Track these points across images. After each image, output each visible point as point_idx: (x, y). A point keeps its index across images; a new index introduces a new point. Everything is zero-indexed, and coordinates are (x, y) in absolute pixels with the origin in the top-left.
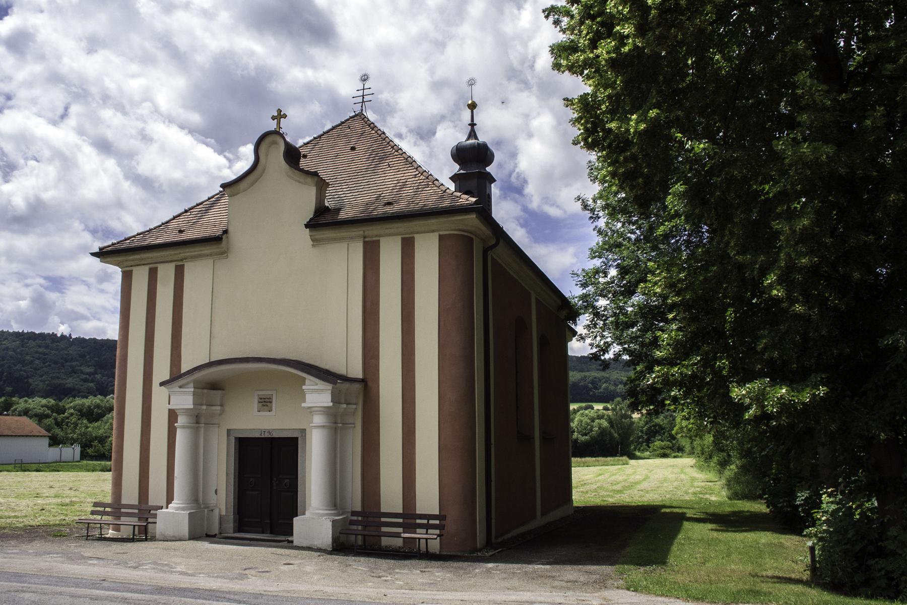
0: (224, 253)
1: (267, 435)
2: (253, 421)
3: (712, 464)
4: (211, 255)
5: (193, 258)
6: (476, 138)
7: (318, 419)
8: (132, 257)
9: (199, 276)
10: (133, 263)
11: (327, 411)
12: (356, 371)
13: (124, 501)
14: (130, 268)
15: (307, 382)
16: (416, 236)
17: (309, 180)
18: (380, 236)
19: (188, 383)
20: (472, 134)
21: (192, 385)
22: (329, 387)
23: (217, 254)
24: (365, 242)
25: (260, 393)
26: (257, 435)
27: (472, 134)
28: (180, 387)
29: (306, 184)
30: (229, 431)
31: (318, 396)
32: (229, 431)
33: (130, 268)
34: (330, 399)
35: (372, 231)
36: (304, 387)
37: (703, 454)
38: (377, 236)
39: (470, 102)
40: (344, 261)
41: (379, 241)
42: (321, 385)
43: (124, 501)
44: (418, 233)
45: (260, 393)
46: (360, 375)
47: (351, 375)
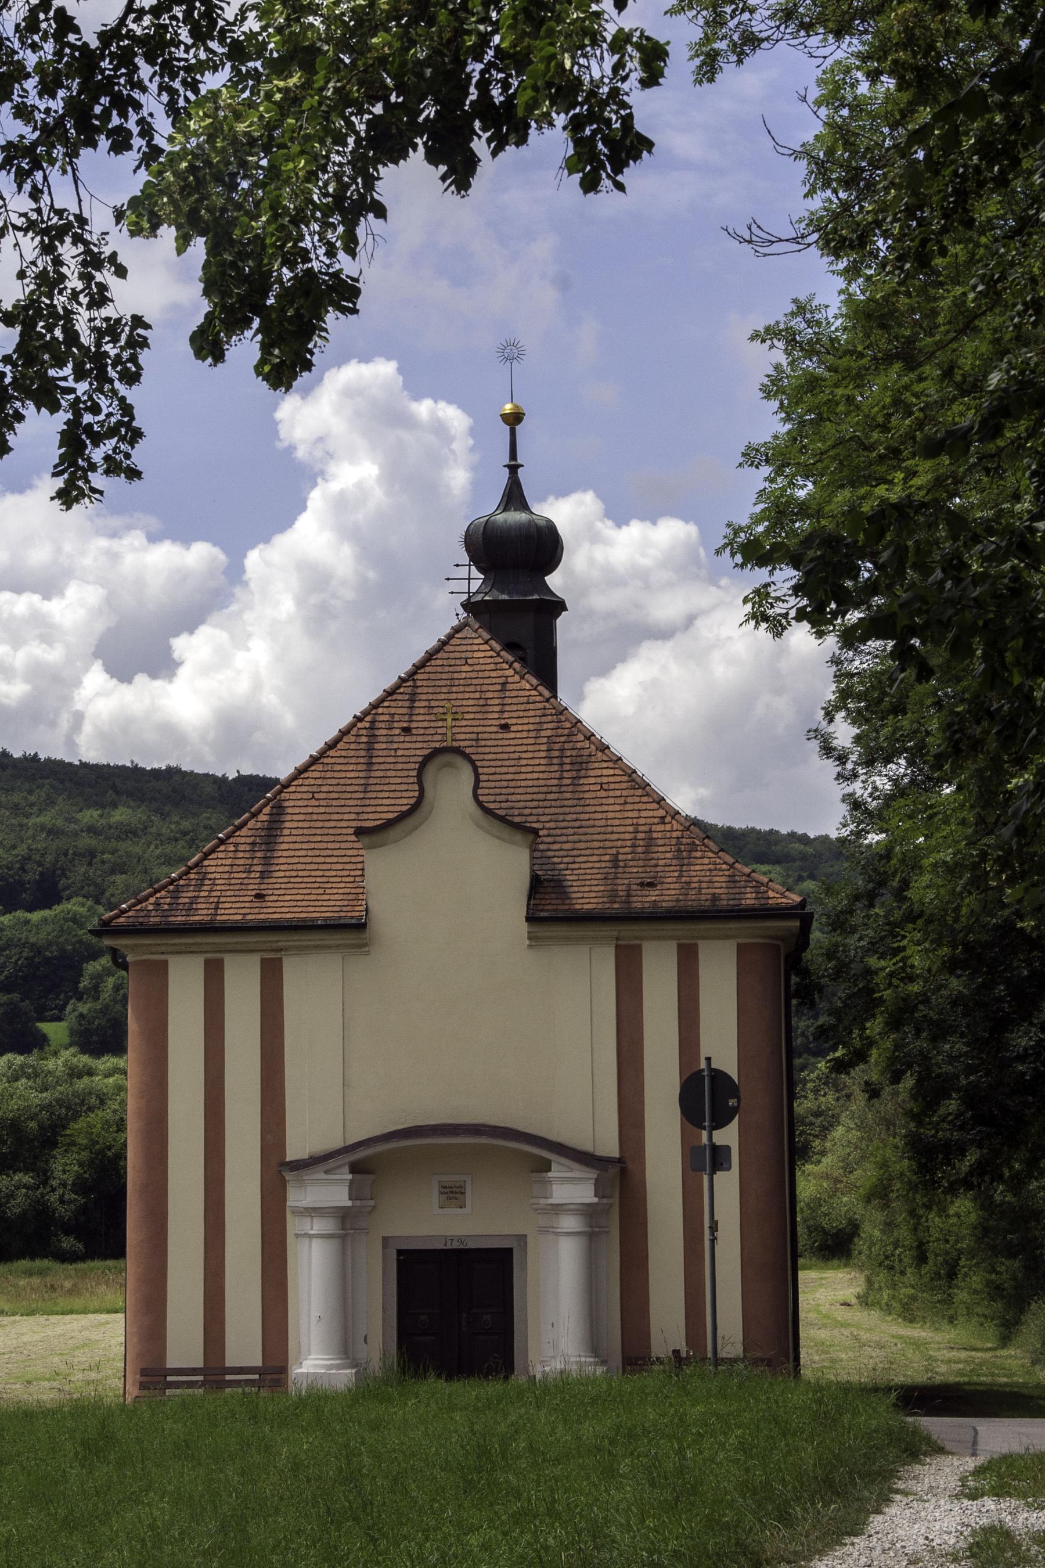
0: (362, 946)
1: (456, 1245)
2: (430, 1221)
3: (962, 1296)
4: (338, 946)
5: (302, 950)
6: (525, 507)
7: (570, 1223)
8: (177, 941)
9: (313, 987)
10: (170, 949)
11: (589, 1212)
12: (609, 1145)
13: (173, 1361)
14: (163, 957)
15: (554, 1166)
16: (700, 943)
17: (518, 837)
18: (642, 938)
19: (340, 1167)
20: (514, 496)
21: (346, 1169)
22: (593, 1174)
23: (349, 946)
24: (617, 947)
25: (445, 1178)
26: (439, 1246)
27: (514, 496)
28: (326, 1172)
29: (513, 843)
30: (385, 1240)
31: (572, 1189)
32: (385, 1240)
33: (163, 957)
34: (592, 1193)
35: (629, 932)
36: (550, 1174)
37: (921, 1258)
38: (636, 938)
39: (508, 408)
40: (583, 977)
41: (639, 947)
42: (578, 1171)
43: (173, 1361)
44: (703, 938)
45: (445, 1178)
46: (615, 1153)
47: (601, 1152)
